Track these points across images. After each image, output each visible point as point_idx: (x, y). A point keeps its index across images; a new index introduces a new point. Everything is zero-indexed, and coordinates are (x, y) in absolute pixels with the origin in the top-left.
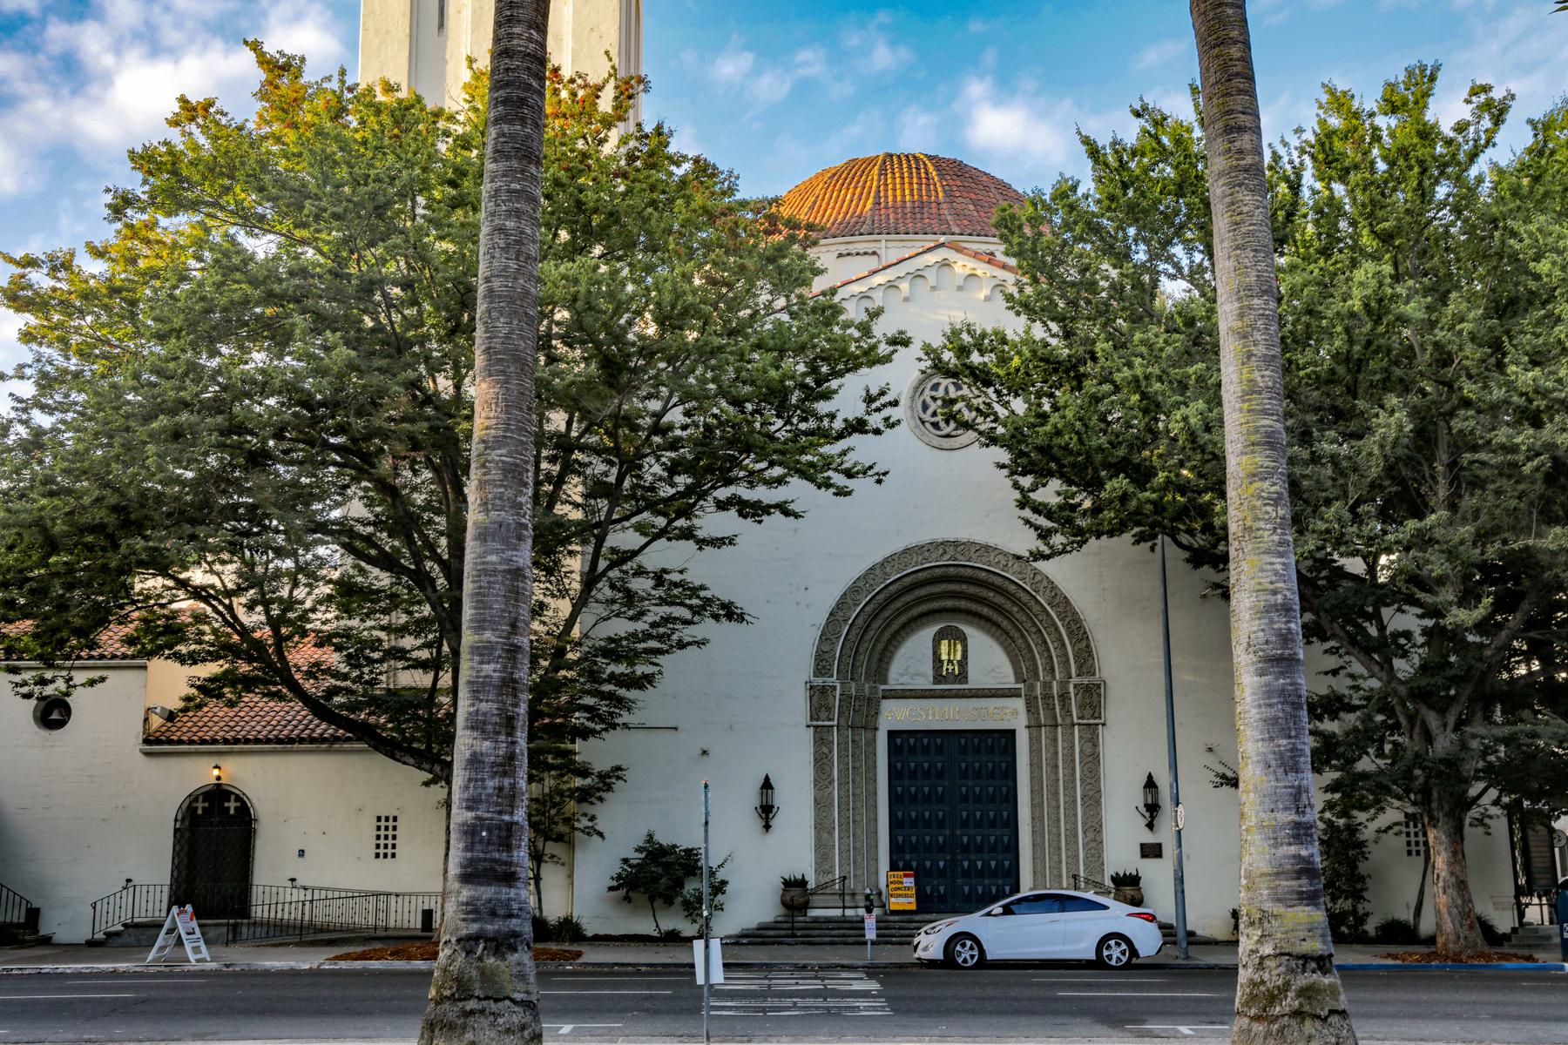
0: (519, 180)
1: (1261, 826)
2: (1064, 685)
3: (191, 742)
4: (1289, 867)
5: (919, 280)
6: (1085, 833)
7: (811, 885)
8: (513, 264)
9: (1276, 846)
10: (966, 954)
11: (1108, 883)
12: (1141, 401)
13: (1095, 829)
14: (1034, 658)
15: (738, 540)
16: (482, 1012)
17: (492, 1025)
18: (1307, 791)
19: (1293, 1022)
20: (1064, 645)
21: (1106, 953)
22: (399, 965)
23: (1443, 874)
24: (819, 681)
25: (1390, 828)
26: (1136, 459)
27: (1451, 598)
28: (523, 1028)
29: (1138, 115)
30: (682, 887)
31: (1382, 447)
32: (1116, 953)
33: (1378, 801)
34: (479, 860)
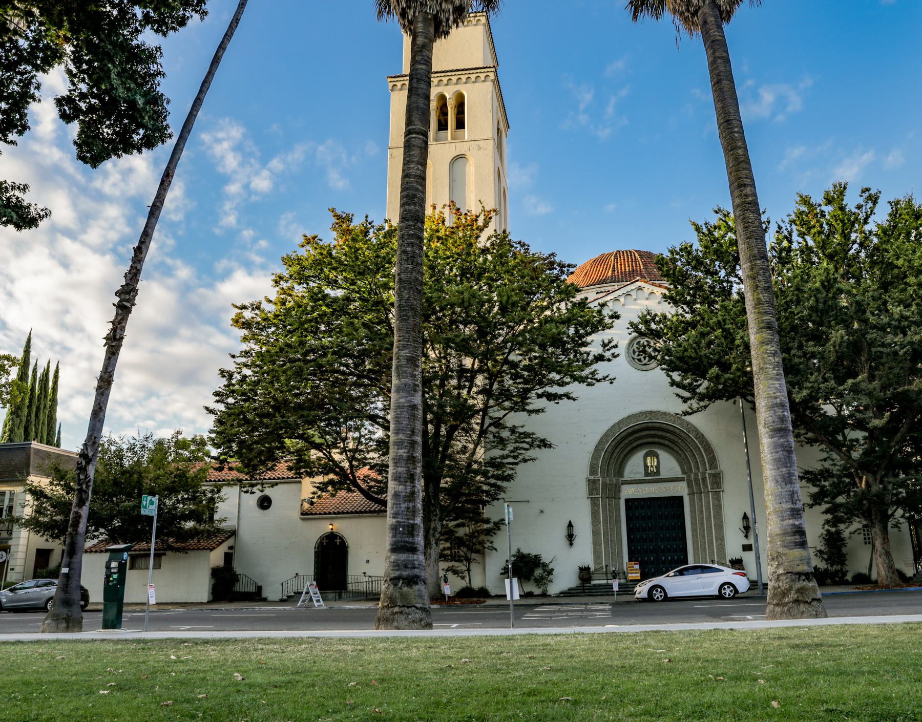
0: (412, 230)
1: (775, 511)
2: (704, 474)
3: (320, 514)
5: (628, 297)
6: (716, 541)
7: (592, 569)
8: (410, 267)
9: (783, 520)
10: (658, 595)
11: (728, 563)
12: (722, 332)
13: (721, 539)
14: (690, 463)
16: (401, 613)
17: (406, 619)
19: (794, 605)
20: (703, 456)
21: (723, 592)
23: (879, 549)
24: (592, 477)
25: (855, 531)
26: (723, 360)
27: (871, 415)
28: (421, 620)
29: (716, 212)
30: (534, 572)
31: (834, 346)
32: (728, 591)
33: (849, 519)
34: (399, 541)
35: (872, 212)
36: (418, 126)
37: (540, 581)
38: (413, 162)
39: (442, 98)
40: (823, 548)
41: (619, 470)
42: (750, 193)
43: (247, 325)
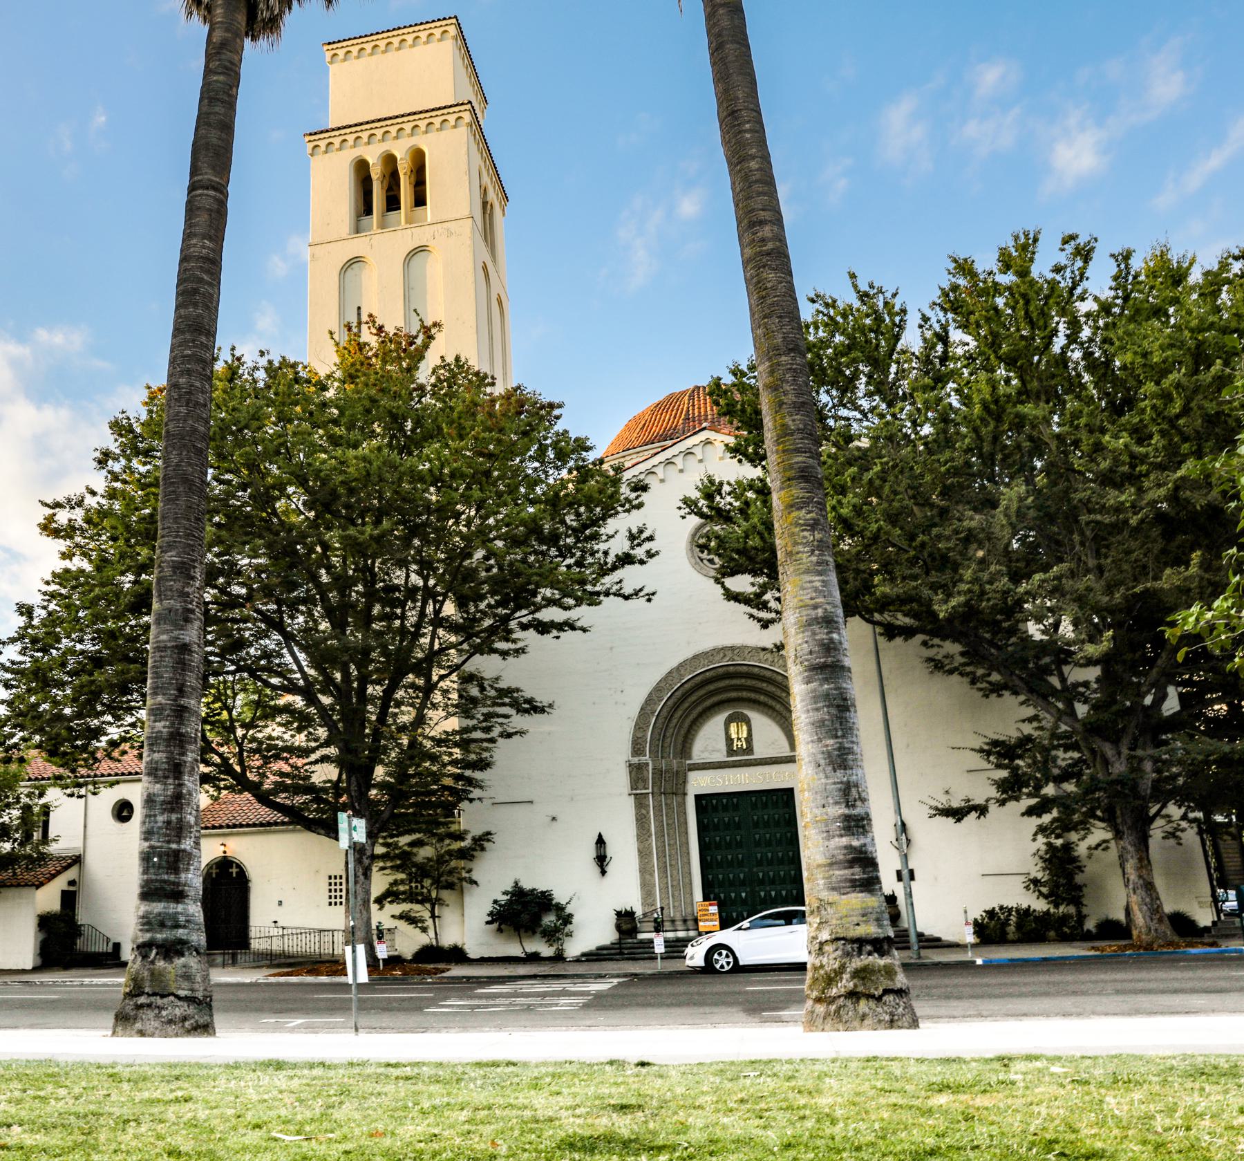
0: (190, 348)
4: (841, 857)
5: (690, 457)
7: (639, 912)
8: (183, 410)
9: (828, 838)
10: (723, 961)
15: (528, 650)
16: (149, 1006)
17: (157, 1016)
18: (857, 786)
19: (849, 1003)
22: (310, 979)
24: (635, 760)
28: (184, 1019)
29: (813, 301)
30: (540, 919)
35: (1082, 275)
36: (208, 176)
37: (552, 935)
38: (195, 235)
39: (390, 160)
40: (1039, 875)
41: (684, 746)
42: (770, 235)
43: (68, 531)
